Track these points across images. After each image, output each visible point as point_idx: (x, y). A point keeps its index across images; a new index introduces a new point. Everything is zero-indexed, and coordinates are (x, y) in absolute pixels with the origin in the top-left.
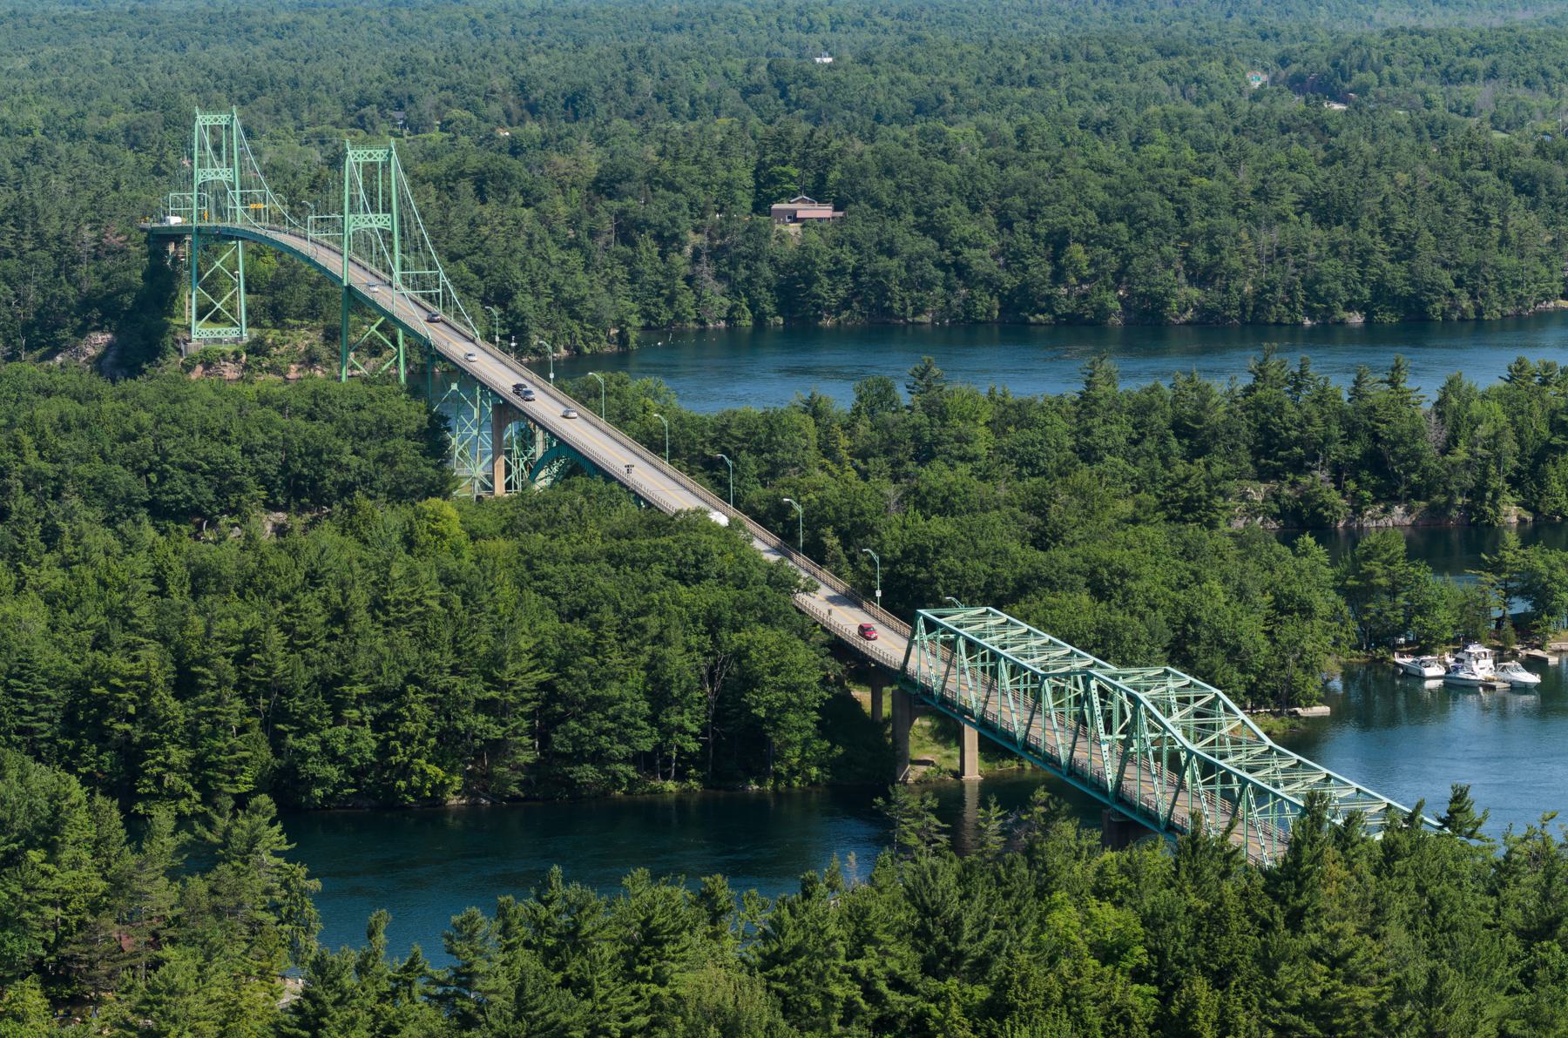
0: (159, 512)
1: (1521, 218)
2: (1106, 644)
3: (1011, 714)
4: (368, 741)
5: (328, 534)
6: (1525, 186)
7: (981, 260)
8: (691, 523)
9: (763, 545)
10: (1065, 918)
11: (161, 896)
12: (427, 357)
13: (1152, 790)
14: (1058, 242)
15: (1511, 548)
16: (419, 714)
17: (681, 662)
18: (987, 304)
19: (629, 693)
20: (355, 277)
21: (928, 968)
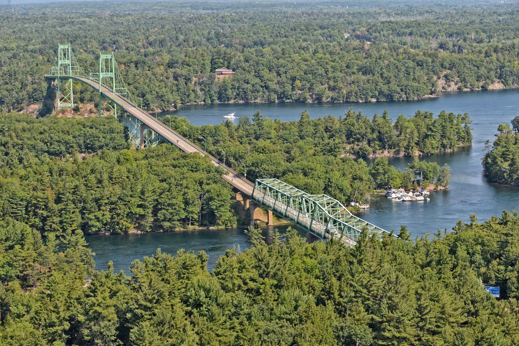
0: (50, 153)
1: (419, 72)
2: (306, 188)
3: (281, 207)
4: (108, 215)
5: (97, 160)
6: (420, 64)
7: (273, 85)
8: (195, 156)
9: (215, 163)
10: (297, 262)
11: (52, 258)
12: (124, 115)
13: (319, 227)
14: (293, 79)
15: (417, 162)
16: (123, 210)
17: (191, 194)
18: (274, 97)
19: (179, 201)
20: (101, 89)
21: (261, 276)
